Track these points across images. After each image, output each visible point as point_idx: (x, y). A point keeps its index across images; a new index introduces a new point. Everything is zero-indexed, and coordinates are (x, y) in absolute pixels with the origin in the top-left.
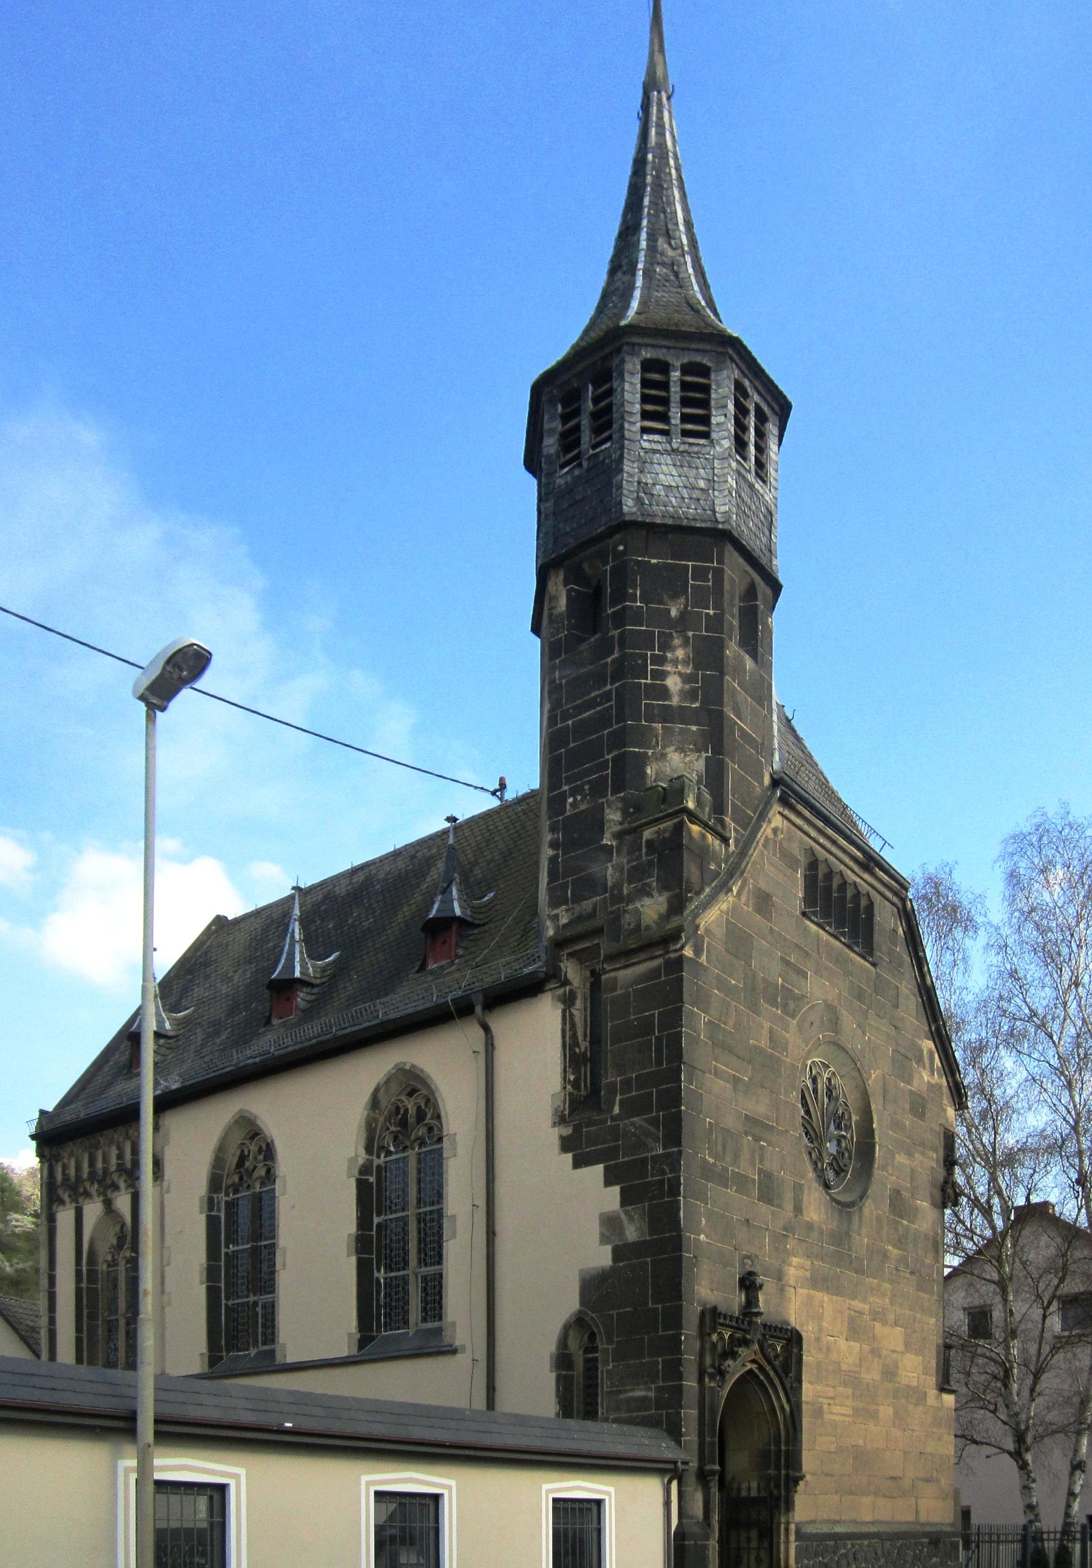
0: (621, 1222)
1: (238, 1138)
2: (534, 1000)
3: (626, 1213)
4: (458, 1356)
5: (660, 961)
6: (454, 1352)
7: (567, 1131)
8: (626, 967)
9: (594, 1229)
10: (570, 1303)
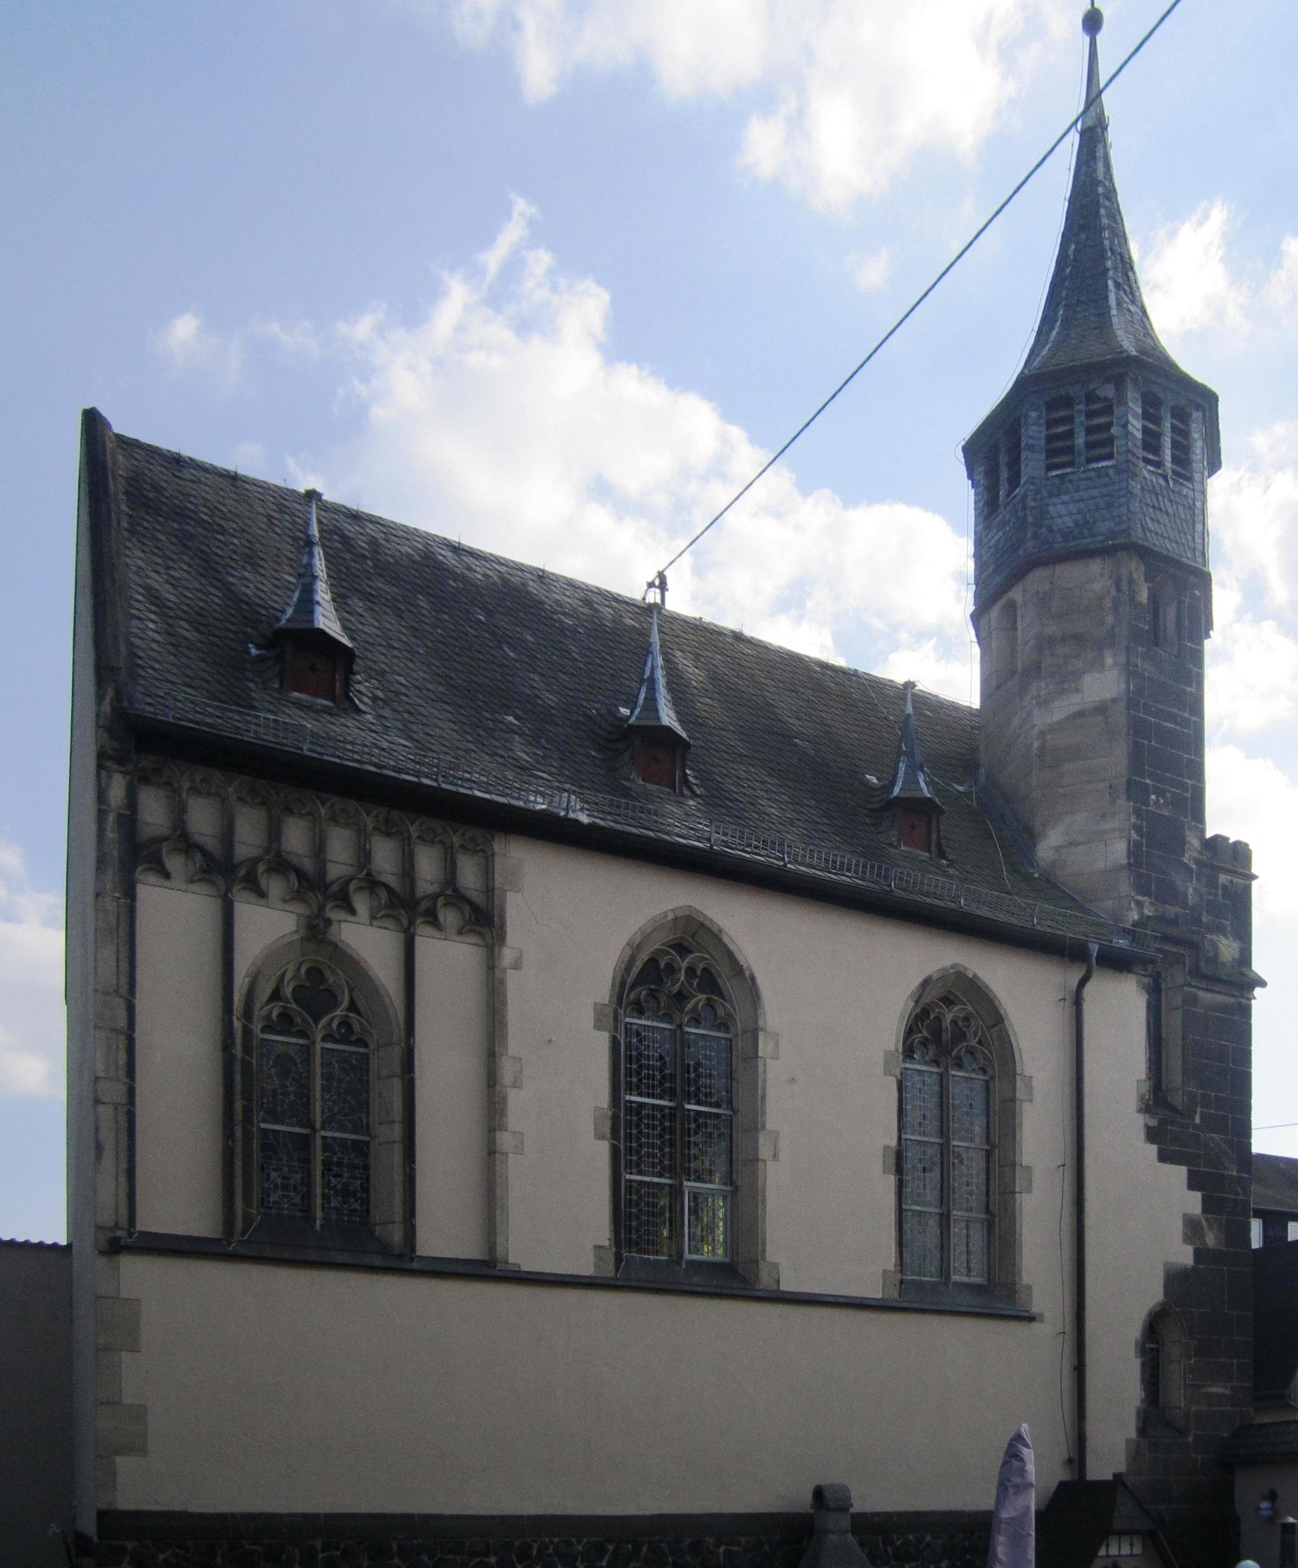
0: (1202, 1228)
1: (375, 923)
2: (1117, 974)
3: (1207, 1220)
4: (1034, 1325)
5: (1232, 1000)
6: (1031, 1319)
7: (1153, 1122)
8: (1207, 990)
9: (1178, 1229)
10: (1154, 1294)
